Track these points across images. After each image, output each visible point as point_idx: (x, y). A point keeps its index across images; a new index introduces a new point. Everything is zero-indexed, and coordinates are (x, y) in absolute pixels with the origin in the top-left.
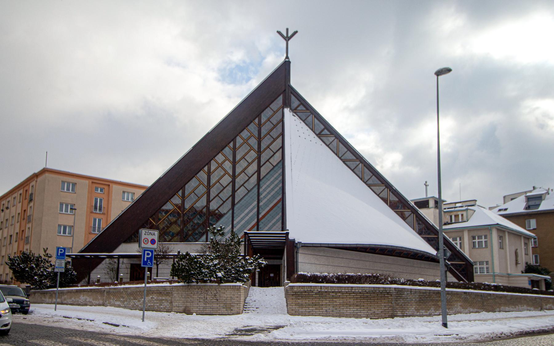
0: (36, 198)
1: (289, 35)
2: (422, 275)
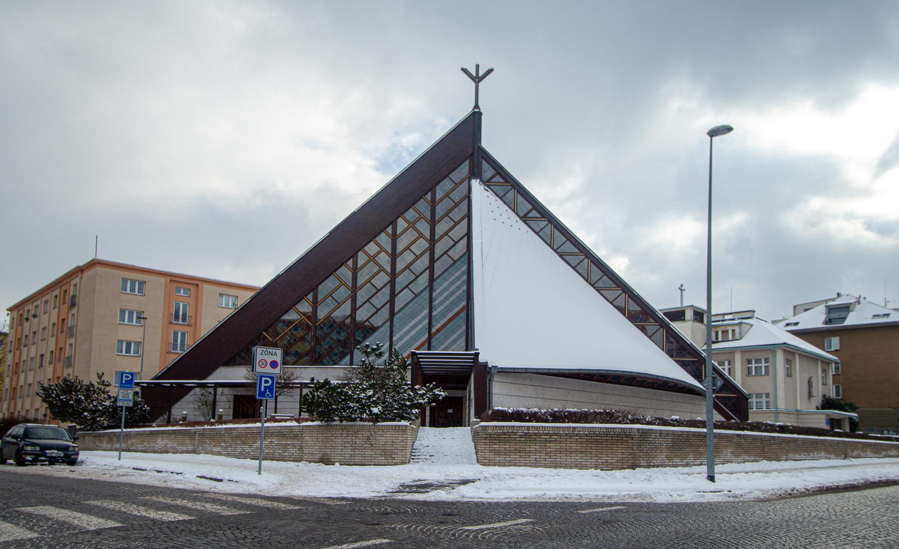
0: (81, 302)
1: (480, 75)
2: (674, 412)
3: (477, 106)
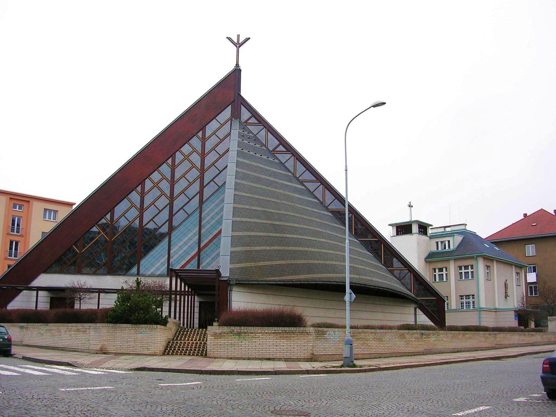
3: (237, 65)
